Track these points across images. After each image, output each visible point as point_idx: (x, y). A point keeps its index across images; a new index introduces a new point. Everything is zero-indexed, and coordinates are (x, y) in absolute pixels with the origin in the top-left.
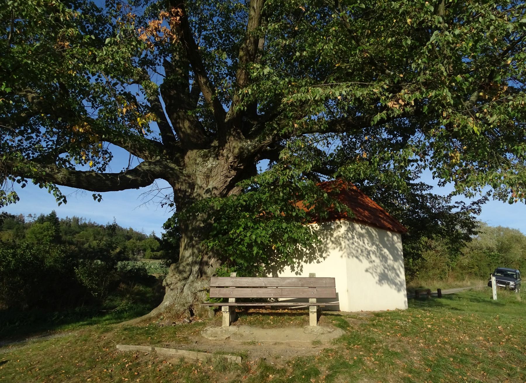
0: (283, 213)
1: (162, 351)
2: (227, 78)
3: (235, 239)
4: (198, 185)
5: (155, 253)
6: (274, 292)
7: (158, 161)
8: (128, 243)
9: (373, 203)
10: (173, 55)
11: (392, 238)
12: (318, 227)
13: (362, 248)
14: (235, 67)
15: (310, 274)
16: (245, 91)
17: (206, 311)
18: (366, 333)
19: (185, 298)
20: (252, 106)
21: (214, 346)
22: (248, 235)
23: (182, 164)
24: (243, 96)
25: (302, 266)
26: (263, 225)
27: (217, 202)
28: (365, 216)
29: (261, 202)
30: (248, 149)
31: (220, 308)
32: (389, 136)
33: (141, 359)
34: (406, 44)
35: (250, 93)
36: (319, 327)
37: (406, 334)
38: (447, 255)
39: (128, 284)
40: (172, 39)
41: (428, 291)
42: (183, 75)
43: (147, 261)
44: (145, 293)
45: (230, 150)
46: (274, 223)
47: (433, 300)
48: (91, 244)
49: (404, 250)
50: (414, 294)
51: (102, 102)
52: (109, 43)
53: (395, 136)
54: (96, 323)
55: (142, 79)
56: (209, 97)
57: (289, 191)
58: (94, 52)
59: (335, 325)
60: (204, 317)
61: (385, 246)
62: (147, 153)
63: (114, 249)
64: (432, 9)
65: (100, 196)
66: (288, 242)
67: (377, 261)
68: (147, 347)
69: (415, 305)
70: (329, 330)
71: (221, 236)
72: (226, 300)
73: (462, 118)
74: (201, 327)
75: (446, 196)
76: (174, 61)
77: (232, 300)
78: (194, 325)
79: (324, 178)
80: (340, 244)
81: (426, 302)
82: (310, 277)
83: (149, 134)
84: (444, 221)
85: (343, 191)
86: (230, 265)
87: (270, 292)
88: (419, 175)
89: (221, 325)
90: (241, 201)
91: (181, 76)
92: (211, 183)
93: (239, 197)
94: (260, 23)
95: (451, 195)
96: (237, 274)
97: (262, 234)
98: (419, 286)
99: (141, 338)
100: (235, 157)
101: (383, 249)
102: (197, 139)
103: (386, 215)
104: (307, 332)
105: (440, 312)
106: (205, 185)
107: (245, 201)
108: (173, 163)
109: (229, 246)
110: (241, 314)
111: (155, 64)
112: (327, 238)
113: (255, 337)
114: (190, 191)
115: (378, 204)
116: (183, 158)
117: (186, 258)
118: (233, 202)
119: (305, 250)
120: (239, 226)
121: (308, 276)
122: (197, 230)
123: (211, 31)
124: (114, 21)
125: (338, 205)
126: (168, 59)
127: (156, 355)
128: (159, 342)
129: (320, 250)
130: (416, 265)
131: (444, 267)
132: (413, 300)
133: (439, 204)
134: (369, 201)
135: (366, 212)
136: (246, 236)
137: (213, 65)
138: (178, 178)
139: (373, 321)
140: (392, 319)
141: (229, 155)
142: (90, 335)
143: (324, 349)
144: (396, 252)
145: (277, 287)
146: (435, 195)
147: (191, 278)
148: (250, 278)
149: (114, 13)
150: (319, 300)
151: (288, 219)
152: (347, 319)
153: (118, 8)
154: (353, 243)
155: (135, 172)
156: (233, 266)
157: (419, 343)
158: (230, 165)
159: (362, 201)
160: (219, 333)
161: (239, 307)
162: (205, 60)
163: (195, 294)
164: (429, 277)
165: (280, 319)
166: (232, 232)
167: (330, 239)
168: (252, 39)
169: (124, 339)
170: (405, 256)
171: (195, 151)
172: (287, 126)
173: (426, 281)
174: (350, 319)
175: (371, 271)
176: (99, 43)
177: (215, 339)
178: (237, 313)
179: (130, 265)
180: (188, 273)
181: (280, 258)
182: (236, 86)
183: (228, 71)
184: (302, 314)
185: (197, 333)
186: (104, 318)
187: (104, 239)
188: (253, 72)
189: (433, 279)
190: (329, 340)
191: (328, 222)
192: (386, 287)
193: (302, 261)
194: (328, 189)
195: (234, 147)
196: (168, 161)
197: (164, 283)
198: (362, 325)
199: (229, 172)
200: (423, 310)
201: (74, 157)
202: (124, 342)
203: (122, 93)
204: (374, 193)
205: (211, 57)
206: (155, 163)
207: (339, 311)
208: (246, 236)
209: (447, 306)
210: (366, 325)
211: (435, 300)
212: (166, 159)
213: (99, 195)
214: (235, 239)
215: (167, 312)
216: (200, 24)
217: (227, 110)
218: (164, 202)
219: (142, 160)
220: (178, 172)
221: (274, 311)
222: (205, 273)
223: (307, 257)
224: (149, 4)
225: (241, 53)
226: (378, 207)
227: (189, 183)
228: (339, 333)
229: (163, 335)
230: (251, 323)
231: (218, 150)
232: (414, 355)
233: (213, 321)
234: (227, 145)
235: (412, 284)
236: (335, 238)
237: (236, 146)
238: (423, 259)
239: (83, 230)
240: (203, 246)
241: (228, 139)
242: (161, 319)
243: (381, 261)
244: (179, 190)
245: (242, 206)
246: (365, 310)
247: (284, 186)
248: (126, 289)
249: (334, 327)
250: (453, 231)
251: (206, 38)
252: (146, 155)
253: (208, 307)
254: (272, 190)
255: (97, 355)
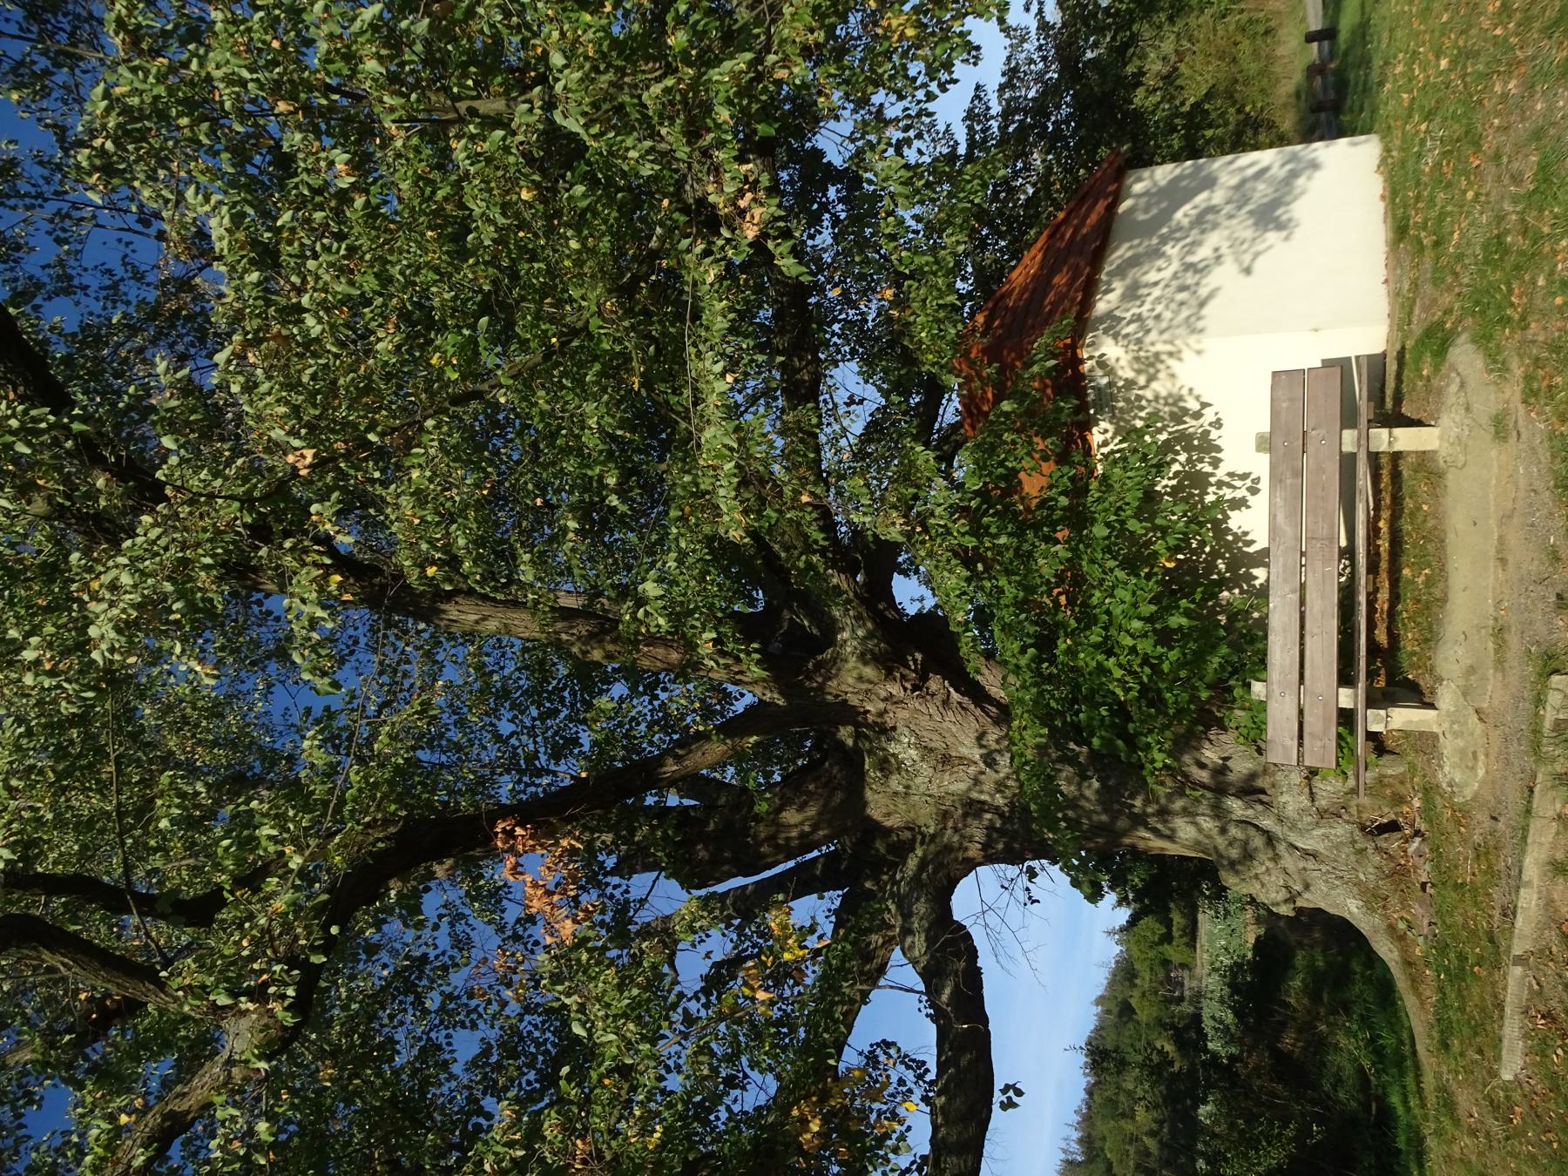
0: (1059, 535)
1: (1528, 930)
2: (663, 696)
3: (1141, 683)
4: (969, 789)
5: (1176, 933)
6: (1318, 564)
7: (899, 907)
8: (1144, 1014)
9: (1026, 260)
10: (601, 850)
11: (1139, 196)
12: (1103, 425)
13: (1172, 289)
14: (631, 674)
15: (1259, 449)
16: (706, 649)
17: (1380, 780)
18: (1465, 267)
19: (1338, 846)
20: (749, 627)
21: (1508, 763)
22: (1129, 642)
23: (907, 835)
24: (723, 654)
25: (1231, 475)
26: (1098, 594)
27: (1027, 734)
28: (1070, 284)
29: (1025, 601)
30: (865, 638)
31: (1371, 736)
32: (825, 223)
33: (1554, 1003)
34: (585, 196)
35: (714, 635)
36: (1445, 420)
37: (1474, 140)
38: (1193, 22)
39: (1283, 1025)
40: (572, 851)
41: (1313, 71)
42: (655, 822)
43: (1203, 957)
44: (1311, 969)
45: (867, 691)
46: (1092, 561)
47: (1346, 54)
48: (1146, 1129)
49: (1176, 158)
50: (1323, 116)
51: (732, 1059)
52: (583, 1025)
53: (824, 207)
54: (1418, 1141)
55: (665, 935)
56: (716, 749)
57: (992, 516)
58: (602, 1069)
59: (1437, 369)
60: (1402, 790)
61: (1166, 216)
62: (876, 939)
63: (1166, 1061)
64: (500, 133)
65: (1007, 1088)
66: (1151, 519)
67: (1214, 239)
68: (1510, 981)
69: (1361, 110)
70: (1454, 388)
71: (1131, 726)
72: (1346, 718)
73: (793, 20)
74: (1438, 801)
75: (1008, 42)
76: (617, 846)
77: (1346, 698)
78: (1431, 822)
79: (950, 410)
80: (1157, 355)
81: (1352, 77)
82: (1270, 450)
83: (820, 931)
84: (1086, 40)
85: (992, 353)
86: (1225, 702)
87: (1319, 575)
88: (941, 127)
89: (1434, 736)
90: (1023, 661)
91: (658, 827)
92: (964, 751)
93: (1011, 667)
94: (515, 604)
95: (1006, 30)
96: (1258, 680)
97: (1128, 598)
98: (1293, 100)
99: (1476, 998)
100: (889, 675)
101: (1173, 224)
102: (835, 789)
103: (1065, 221)
104: (1461, 458)
105: (1391, 30)
106: (972, 770)
107: (1023, 651)
108: (905, 863)
109: (1163, 701)
110: (1394, 673)
111: (627, 901)
112: (1139, 398)
113: (1479, 628)
114: (988, 816)
115: (1029, 246)
116: (889, 831)
117: (1201, 838)
118: (1023, 687)
119: (1176, 467)
120: (1102, 670)
121: (1265, 458)
122: (1109, 796)
123: (539, 739)
124: (514, 1008)
125: (1036, 369)
126: (611, 862)
127: (1541, 951)
128: (1491, 940)
129: (1178, 418)
130: (1222, 115)
131: (1231, 28)
132: (1346, 118)
133: (1031, 61)
134: (1021, 274)
135: (1056, 280)
136: (1133, 650)
137: (626, 736)
138: (948, 848)
139: (1422, 248)
140: (1418, 184)
141: (883, 694)
142: (1463, 1161)
143: (1524, 402)
144: (1184, 183)
145: (1302, 554)
146: (1003, 74)
147: (1267, 823)
148: (1271, 638)
149: (495, 1007)
150: (1349, 418)
151: (1078, 519)
152: (1417, 329)
153: (483, 995)
154: (1158, 317)
155: (932, 977)
156: (1230, 690)
157: (1505, 96)
158: (913, 691)
159: (1022, 293)
160: (1460, 743)
161: (1371, 675)
162: (613, 759)
163: (1322, 814)
164: (1263, 72)
165: (1415, 546)
166: (1119, 692)
167: (1141, 388)
168: (559, 625)
169: (1480, 1052)
170: (1195, 154)
171: (869, 794)
172: (799, 524)
173: (1278, 80)
174: (1415, 320)
175: (1247, 258)
176: (581, 1054)
177: (1482, 757)
178: (1388, 683)
179: (1216, 1013)
180: (1252, 831)
181: (1202, 544)
182: (688, 669)
183: (644, 693)
184: (1396, 476)
185: (1462, 814)
186: (1400, 1110)
187: (1130, 1087)
188: (658, 626)
189: (1271, 59)
190: (1493, 388)
191: (1087, 395)
192: (1299, 209)
193: (1212, 475)
194: (984, 398)
195: (860, 679)
196: (898, 877)
197: (1285, 910)
198: (1437, 282)
199: (933, 695)
200: (1381, 84)
201: (891, 1156)
202: (1489, 1054)
203: (703, 1000)
204: (996, 261)
205: (607, 740)
206: (907, 915)
207: (1384, 355)
208: (1133, 650)
209: (1368, 9)
210: (1435, 270)
211: (1343, 46)
212: (895, 883)
213: (1004, 1091)
214: (1141, 683)
215: (1384, 907)
216: (521, 772)
217: (749, 699)
218: (1021, 896)
219: (897, 955)
220: (932, 848)
221: (1384, 565)
222: (1253, 776)
223: (1201, 460)
224: (467, 911)
225: (597, 655)
226: (1039, 244)
227: (965, 815)
228: (1465, 356)
229: (1465, 926)
230: (1427, 640)
231: (867, 726)
232: (1551, 108)
233: (1419, 761)
234: (854, 700)
235: (1287, 123)
236: (1139, 372)
237: (855, 674)
238: (1209, 96)
239: (1102, 1150)
240: (1162, 784)
241: (837, 696)
242: (1410, 928)
243: (1215, 226)
244: (985, 847)
245: (1038, 660)
246: (1380, 272)
247: (977, 530)
248: (1300, 1031)
249: (1444, 371)
250: (1118, 10)
251: (556, 756)
252: (880, 941)
253: (1368, 774)
254: (987, 569)
255: (1540, 1145)
